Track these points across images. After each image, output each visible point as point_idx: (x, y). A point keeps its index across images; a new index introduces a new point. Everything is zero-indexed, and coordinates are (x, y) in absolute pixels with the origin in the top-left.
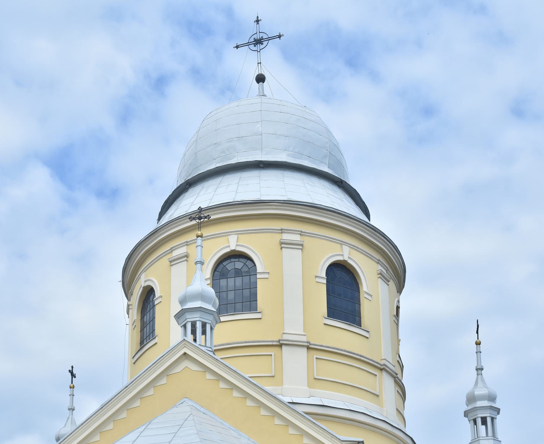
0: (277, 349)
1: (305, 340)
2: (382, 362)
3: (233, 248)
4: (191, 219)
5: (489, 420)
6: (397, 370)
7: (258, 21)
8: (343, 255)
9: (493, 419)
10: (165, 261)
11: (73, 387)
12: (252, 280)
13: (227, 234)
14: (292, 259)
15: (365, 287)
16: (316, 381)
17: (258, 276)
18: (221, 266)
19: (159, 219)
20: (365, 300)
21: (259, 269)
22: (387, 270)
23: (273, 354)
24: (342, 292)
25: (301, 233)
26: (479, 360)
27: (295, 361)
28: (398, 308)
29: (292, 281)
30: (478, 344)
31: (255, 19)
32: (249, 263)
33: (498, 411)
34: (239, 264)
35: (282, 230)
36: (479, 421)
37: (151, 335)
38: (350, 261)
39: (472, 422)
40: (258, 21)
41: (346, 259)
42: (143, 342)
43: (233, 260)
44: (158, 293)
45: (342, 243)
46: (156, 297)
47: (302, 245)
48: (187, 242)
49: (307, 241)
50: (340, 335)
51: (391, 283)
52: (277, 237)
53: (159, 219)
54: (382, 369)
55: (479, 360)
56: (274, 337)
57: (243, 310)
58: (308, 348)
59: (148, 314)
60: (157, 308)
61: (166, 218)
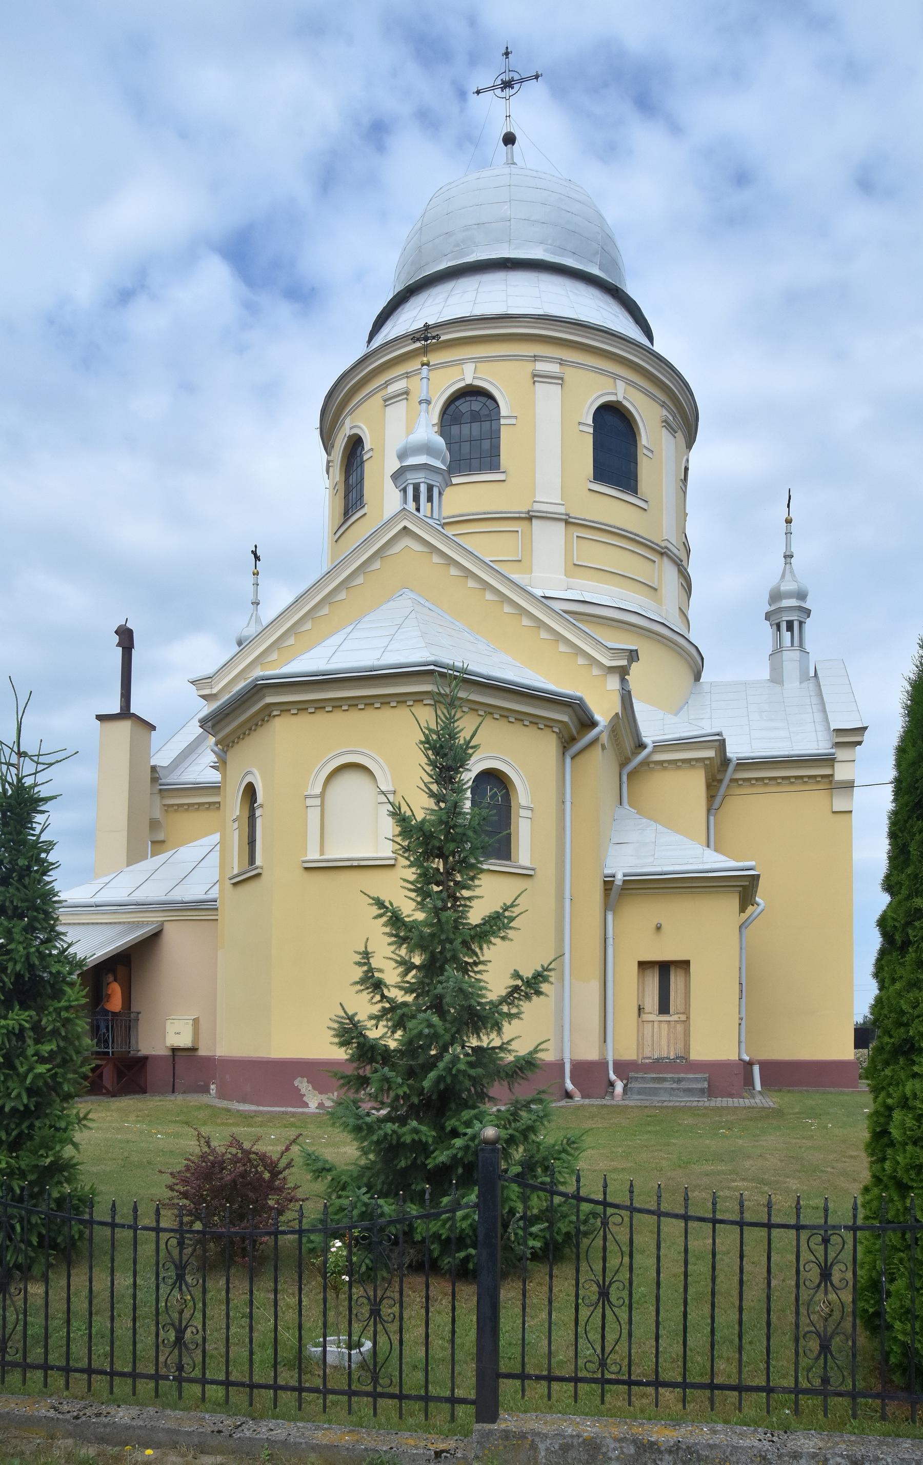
0: (525, 524)
1: (563, 512)
2: (663, 544)
3: (469, 381)
4: (415, 339)
5: (796, 624)
6: (683, 555)
7: (507, 54)
8: (616, 394)
9: (801, 623)
10: (377, 399)
11: (258, 574)
12: (493, 428)
13: (461, 362)
14: (548, 400)
15: (644, 439)
16: (576, 568)
17: (502, 421)
18: (453, 407)
19: (369, 341)
20: (645, 458)
21: (504, 411)
22: (674, 417)
23: (519, 530)
24: (614, 447)
25: (562, 362)
26: (788, 544)
27: (549, 541)
28: (686, 469)
29: (546, 428)
30: (789, 521)
31: (504, 51)
32: (490, 402)
33: (808, 612)
34: (476, 404)
35: (535, 356)
36: (784, 626)
37: (359, 503)
38: (626, 403)
39: (775, 627)
40: (507, 54)
41: (620, 399)
42: (347, 513)
43: (468, 398)
44: (367, 445)
45: (615, 377)
46: (366, 449)
47: (562, 379)
48: (407, 373)
49: (570, 374)
50: (609, 507)
51: (679, 435)
52: (529, 367)
53: (369, 341)
54: (663, 553)
55: (788, 544)
56: (522, 507)
57: (481, 469)
58: (567, 523)
59: (355, 474)
60: (367, 467)
61: (392, 330)
